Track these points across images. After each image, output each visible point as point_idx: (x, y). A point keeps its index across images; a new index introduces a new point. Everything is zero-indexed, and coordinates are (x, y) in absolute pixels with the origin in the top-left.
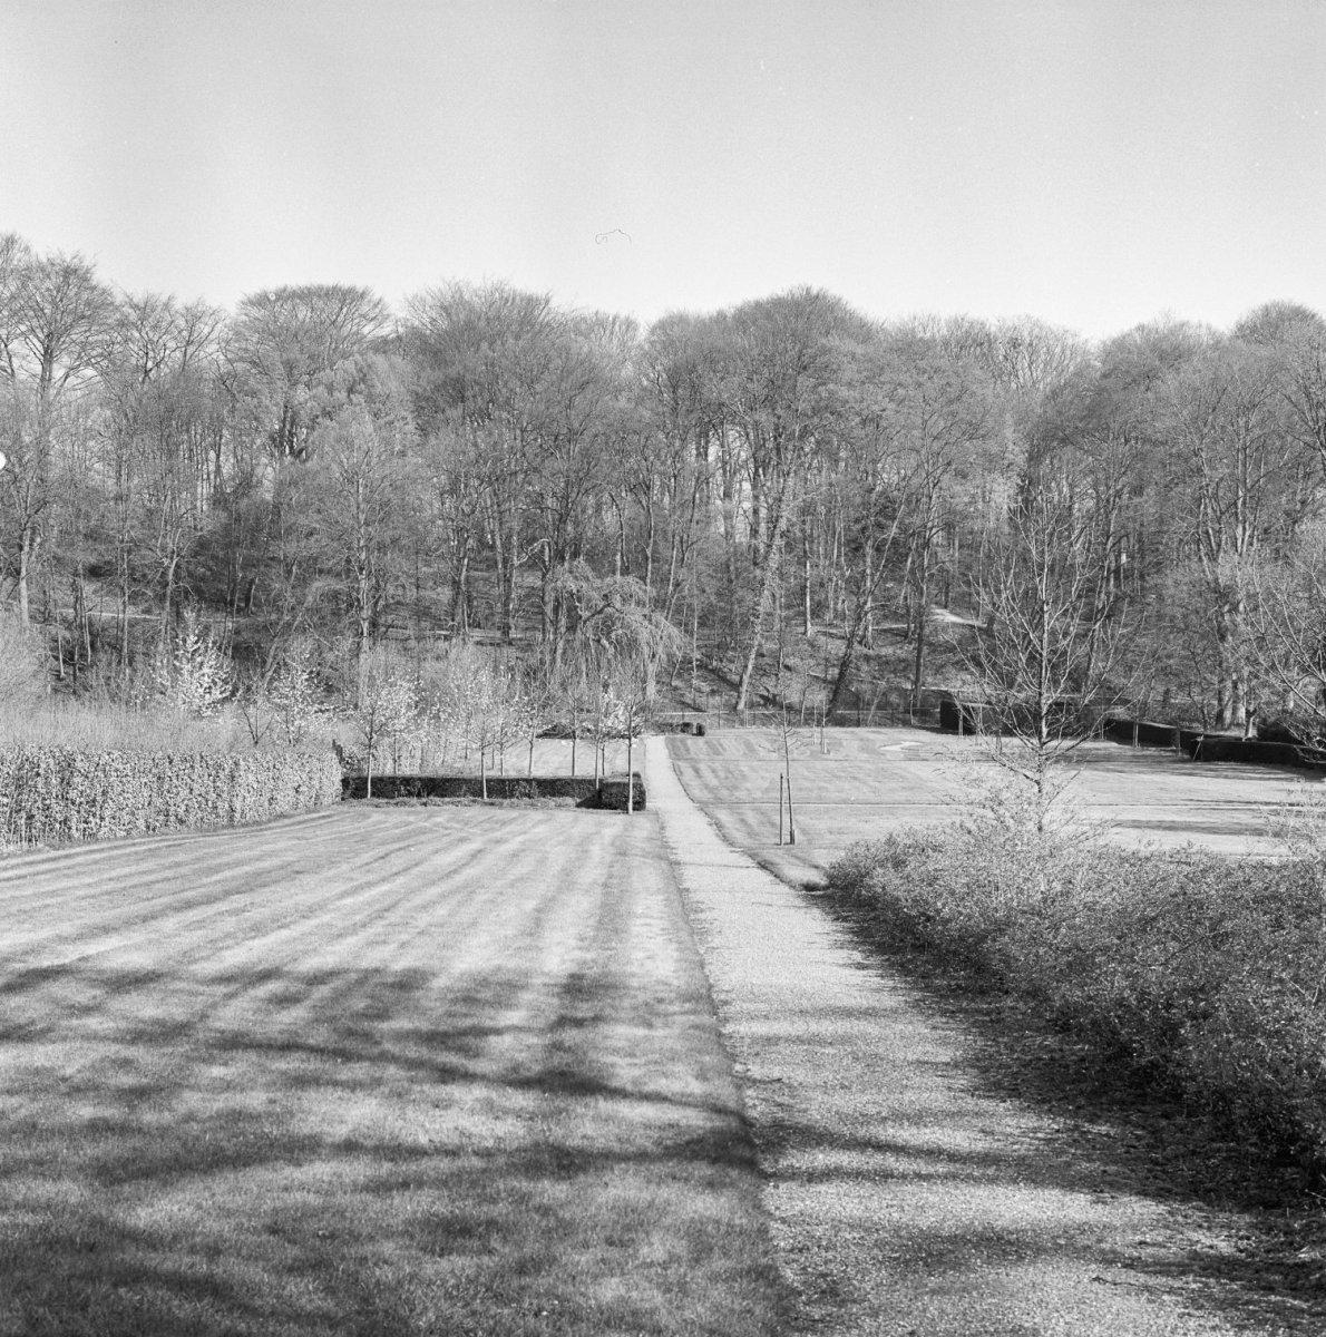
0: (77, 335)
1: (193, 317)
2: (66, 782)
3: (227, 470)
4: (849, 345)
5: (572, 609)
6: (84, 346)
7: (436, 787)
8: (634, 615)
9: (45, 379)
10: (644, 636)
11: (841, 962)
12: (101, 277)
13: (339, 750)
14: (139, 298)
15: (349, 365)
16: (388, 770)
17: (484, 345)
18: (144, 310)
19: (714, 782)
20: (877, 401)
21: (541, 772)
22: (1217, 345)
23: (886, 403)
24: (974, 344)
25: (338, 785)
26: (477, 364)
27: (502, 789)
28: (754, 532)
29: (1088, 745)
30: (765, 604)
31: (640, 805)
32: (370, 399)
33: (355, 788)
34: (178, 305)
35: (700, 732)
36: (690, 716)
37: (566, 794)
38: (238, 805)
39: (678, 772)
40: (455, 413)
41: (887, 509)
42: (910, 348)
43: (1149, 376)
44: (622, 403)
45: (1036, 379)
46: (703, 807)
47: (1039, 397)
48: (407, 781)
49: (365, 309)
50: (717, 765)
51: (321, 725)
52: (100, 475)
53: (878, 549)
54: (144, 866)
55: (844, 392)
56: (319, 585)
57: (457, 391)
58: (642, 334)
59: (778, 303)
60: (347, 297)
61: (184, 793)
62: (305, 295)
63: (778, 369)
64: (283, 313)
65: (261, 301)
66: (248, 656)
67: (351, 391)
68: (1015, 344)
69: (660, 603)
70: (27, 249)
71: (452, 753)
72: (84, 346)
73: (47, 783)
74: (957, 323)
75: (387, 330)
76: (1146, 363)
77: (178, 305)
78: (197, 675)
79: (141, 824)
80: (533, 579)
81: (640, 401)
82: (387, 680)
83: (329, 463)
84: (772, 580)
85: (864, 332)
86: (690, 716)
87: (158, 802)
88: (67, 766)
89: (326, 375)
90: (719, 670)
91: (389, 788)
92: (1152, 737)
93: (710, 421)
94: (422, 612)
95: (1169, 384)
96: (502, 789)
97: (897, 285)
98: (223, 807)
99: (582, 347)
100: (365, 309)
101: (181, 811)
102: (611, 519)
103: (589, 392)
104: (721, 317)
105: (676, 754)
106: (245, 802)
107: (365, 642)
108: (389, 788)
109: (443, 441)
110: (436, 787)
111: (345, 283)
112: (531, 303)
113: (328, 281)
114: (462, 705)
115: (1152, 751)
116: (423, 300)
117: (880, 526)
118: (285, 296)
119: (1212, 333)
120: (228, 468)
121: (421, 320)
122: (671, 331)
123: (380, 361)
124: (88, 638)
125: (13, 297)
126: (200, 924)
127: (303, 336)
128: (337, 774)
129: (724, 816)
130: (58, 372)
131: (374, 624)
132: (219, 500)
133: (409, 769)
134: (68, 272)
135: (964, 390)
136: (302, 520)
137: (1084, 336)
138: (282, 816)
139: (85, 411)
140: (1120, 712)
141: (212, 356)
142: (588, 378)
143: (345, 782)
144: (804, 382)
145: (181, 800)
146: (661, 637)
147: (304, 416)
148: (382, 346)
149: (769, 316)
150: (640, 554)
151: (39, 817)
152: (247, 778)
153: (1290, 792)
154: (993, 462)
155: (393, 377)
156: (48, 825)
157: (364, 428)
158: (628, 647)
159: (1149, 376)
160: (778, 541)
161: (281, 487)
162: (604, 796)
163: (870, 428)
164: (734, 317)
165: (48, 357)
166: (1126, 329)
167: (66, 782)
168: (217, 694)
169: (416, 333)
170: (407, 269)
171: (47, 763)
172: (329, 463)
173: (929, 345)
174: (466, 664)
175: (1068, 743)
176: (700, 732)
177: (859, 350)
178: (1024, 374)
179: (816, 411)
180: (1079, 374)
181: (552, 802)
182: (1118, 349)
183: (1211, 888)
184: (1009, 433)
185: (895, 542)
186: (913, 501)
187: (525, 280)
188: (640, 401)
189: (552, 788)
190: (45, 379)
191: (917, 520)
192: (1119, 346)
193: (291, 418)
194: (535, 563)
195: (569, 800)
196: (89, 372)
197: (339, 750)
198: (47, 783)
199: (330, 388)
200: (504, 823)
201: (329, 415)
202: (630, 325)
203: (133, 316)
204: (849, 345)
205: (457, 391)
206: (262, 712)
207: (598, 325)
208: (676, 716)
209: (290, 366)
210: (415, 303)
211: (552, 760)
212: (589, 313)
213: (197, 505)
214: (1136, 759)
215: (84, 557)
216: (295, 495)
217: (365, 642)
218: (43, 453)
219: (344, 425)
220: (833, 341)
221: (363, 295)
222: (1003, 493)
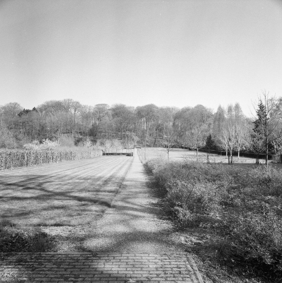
0: (78, 109)
1: (90, 107)
3: (93, 122)
4: (156, 109)
5: (128, 136)
7: (112, 154)
8: (134, 136)
9: (75, 113)
10: (135, 139)
11: (139, 171)
13: (102, 150)
14: (84, 105)
16: (108, 152)
18: (85, 106)
19: (141, 153)
20: (158, 115)
21: (123, 152)
24: (168, 109)
25: (102, 154)
26: (119, 112)
27: (119, 154)
30: (147, 135)
31: (132, 156)
32: (108, 115)
33: (104, 154)
34: (88, 106)
35: (141, 148)
36: (140, 147)
38: (91, 156)
39: (137, 152)
40: (116, 116)
41: (159, 126)
42: (162, 109)
43: (186, 112)
44: (133, 115)
45: (174, 112)
46: (139, 156)
47: (175, 114)
48: (109, 153)
49: (107, 106)
51: (101, 148)
52: (81, 123)
53: (159, 129)
58: (135, 108)
59: (149, 105)
60: (106, 105)
61: (85, 155)
62: (101, 105)
63: (147, 113)
64: (99, 106)
65: (97, 105)
66: (94, 141)
67: (106, 114)
68: (172, 109)
69: (136, 135)
71: (114, 151)
73: (69, 154)
75: (109, 108)
76: (185, 111)
77: (88, 106)
78: (88, 143)
80: (124, 133)
82: (108, 144)
83: (103, 121)
84: (148, 133)
85: (157, 108)
86: (140, 147)
87: (82, 156)
88: (71, 153)
89: (103, 113)
91: (107, 154)
92: (186, 148)
93: (142, 117)
94: (113, 136)
95: (187, 112)
96: (119, 154)
98: (89, 157)
99: (129, 110)
100: (107, 106)
104: (143, 106)
105: (138, 150)
108: (107, 154)
109: (115, 119)
110: (112, 154)
111: (105, 103)
112: (124, 105)
113: (103, 103)
114: (116, 146)
115: (186, 150)
118: (99, 105)
119: (192, 107)
120: (94, 122)
121: (113, 107)
122: (138, 108)
123: (109, 111)
126: (79, 169)
127: (100, 110)
128: (102, 153)
129: (141, 157)
130: (76, 112)
131: (108, 138)
132: (93, 125)
134: (77, 103)
135: (167, 114)
136: (100, 127)
139: (79, 116)
141: (92, 111)
142: (130, 113)
143: (103, 154)
144: (151, 113)
145: (84, 155)
146: (136, 139)
147: (101, 117)
148: (109, 110)
150: (134, 130)
151: (68, 158)
153: (18, 173)
155: (110, 113)
156: (69, 159)
157: (107, 118)
158: (133, 140)
159: (186, 112)
161: (99, 124)
162: (128, 155)
163: (158, 117)
165: (75, 111)
168: (90, 145)
170: (111, 102)
172: (103, 121)
173: (163, 109)
174: (117, 142)
175: (172, 149)
176: (141, 148)
177: (157, 110)
178: (173, 112)
179: (152, 116)
180: (179, 112)
181: (123, 155)
184: (172, 118)
186: (162, 125)
189: (123, 154)
190: (75, 113)
192: (183, 109)
193: (100, 116)
194: (124, 131)
196: (79, 112)
197: (102, 150)
198: (69, 154)
199: (104, 114)
201: (104, 117)
203: (84, 107)
204: (156, 109)
206: (95, 147)
207: (130, 107)
208: (138, 146)
209: (100, 112)
211: (125, 151)
212: (130, 106)
213: (90, 126)
214: (183, 151)
215: (79, 131)
216: (100, 125)
217: (107, 139)
218: (75, 121)
219: (105, 118)
220: (154, 109)
222: (171, 124)
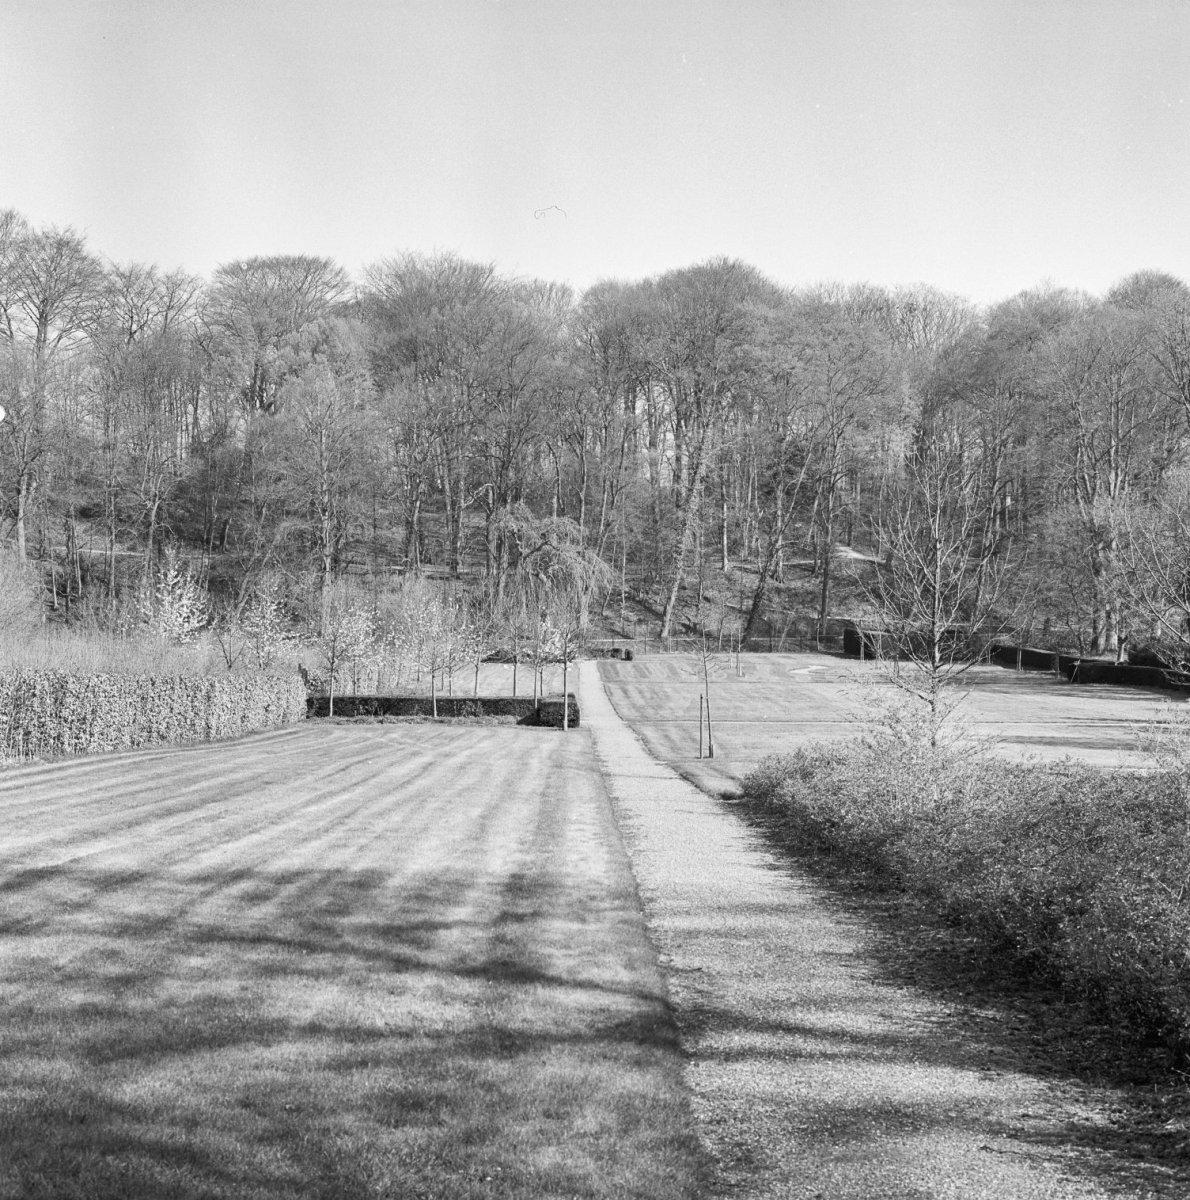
0: (69, 300)
1: (174, 284)
2: (59, 702)
3: (203, 422)
4: (762, 310)
5: (513, 547)
6: (75, 310)
7: (391, 707)
8: (569, 552)
9: (41, 340)
10: (578, 571)
11: (755, 864)
12: (90, 249)
13: (304, 673)
14: (124, 268)
15: (314, 328)
16: (349, 691)
17: (435, 310)
18: (129, 278)
19: (641, 702)
20: (787, 360)
21: (485, 693)
22: (1092, 309)
23: (795, 362)
24: (874, 309)
25: (304, 705)
26: (428, 327)
27: (450, 708)
28: (677, 478)
29: (976, 669)
30: (686, 542)
31: (574, 722)
32: (332, 358)
33: (318, 707)
34: (160, 274)
35: (629, 657)
36: (619, 643)
37: (508, 713)
38: (213, 722)
39: (608, 693)
40: (408, 371)
41: (796, 457)
42: (817, 312)
43: (1032, 337)
44: (559, 362)
45: (929, 340)
46: (631, 724)
47: (932, 357)
48: (365, 701)
49: (327, 277)
50: (643, 687)
51: (288, 651)
52: (90, 426)
53: (788, 493)
54: (129, 777)
55: (757, 352)
56: (287, 525)
57: (410, 351)
58: (576, 300)
59: (698, 272)
60: (312, 267)
61: (165, 712)
62: (274, 265)
63: (698, 331)
64: (254, 281)
65: (234, 270)
66: (223, 589)
67: (315, 351)
68: (911, 308)
69: (592, 541)
70: (24, 224)
71: (406, 676)
72: (75, 310)
73: (42, 703)
74: (859, 290)
75: (347, 296)
76: (1028, 326)
77: (160, 274)
78: (176, 606)
79: (127, 739)
80: (478, 520)
81: (574, 360)
82: (347, 610)
83: (295, 416)
84: (692, 521)
85: (775, 298)
86: (619, 643)
87: (142, 719)
88: (60, 688)
89: (293, 337)
90: (645, 602)
91: (349, 708)
92: (1034, 662)
93: (637, 378)
94: (379, 549)
95: (1049, 344)
96: (450, 708)
97: (805, 255)
98: (200, 724)
99: (522, 311)
100: (327, 277)
101: (162, 728)
102: (548, 465)
103: (529, 352)
104: (647, 284)
105: (607, 676)
106: (220, 720)
107: (328, 576)
108: (349, 708)
109: (397, 396)
110: (391, 707)
111: (310, 254)
112: (476, 272)
113: (294, 252)
114: (415, 633)
115: (1034, 674)
116: (380, 270)
117: (790, 472)
118: (255, 265)
119: (1088, 299)
120: (204, 420)
121: (378, 287)
122: (602, 297)
123: (341, 324)
124: (79, 573)
125: (12, 267)
126: (180, 829)
127: (272, 302)
128: (302, 694)
129: (649, 732)
130: (52, 334)
131: (336, 560)
132: (196, 449)
133: (367, 690)
134: (61, 244)
135: (865, 350)
136: (271, 467)
137: (973, 302)
138: (253, 732)
139: (76, 369)
140: (1005, 639)
141: (190, 319)
142: (527, 339)
143: (310, 702)
144: (722, 343)
145: (162, 718)
146: (593, 571)
147: (273, 374)
148: (343, 310)
149: (690, 284)
150: (574, 497)
151: (35, 733)
152: (222, 698)
154: (891, 415)
155: (353, 339)
156: (43, 741)
157: (327, 384)
158: (564, 580)
159: (1032, 337)
160: (699, 486)
161: (252, 437)
162: (542, 714)
163: (781, 384)
164: (659, 284)
165: (43, 320)
166: (1011, 296)
167: (59, 702)
168: (194, 623)
169: (373, 299)
170: (366, 241)
171: (42, 685)
172: (295, 416)
173: (833, 309)
174: (419, 596)
175: (958, 667)
176: (629, 657)
177: (771, 314)
178: (919, 336)
179: (732, 369)
180: (968, 335)
181: (495, 719)
182: (1003, 313)
183: (1087, 797)
184: (905, 389)
185: (803, 486)
186: (820, 450)
187: (471, 252)
188: (574, 360)
189: (495, 707)
190: (41, 340)
191: (823, 467)
192: (1005, 311)
193: (261, 375)
194: (480, 505)
195: (511, 718)
196: (80, 334)
197: (304, 673)
198: (42, 703)
199: (297, 349)
200: (452, 739)
201: (295, 372)
202: (565, 292)
203: (120, 284)
204: (762, 310)
205: (410, 351)
206: (235, 639)
207: (537, 292)
208: (607, 642)
209: (260, 329)
210: (372, 272)
211: (496, 682)
212: (528, 280)
213: (177, 454)
214: (1019, 682)
215: (76, 500)
216: (265, 445)
217: (328, 576)
218: (39, 406)
219: (309, 381)
220: (748, 306)
221: (325, 265)
222: (900, 443)
